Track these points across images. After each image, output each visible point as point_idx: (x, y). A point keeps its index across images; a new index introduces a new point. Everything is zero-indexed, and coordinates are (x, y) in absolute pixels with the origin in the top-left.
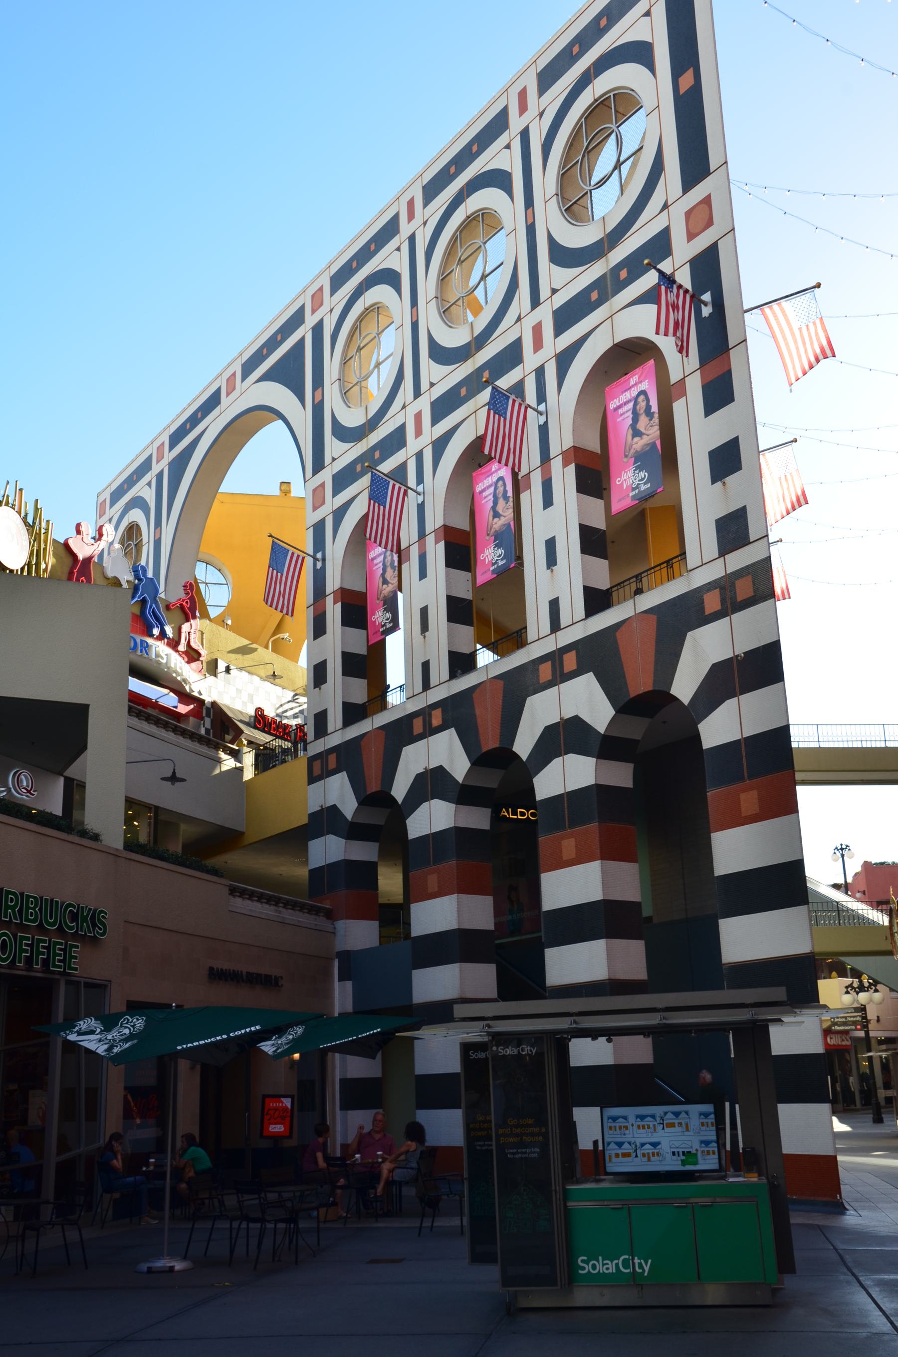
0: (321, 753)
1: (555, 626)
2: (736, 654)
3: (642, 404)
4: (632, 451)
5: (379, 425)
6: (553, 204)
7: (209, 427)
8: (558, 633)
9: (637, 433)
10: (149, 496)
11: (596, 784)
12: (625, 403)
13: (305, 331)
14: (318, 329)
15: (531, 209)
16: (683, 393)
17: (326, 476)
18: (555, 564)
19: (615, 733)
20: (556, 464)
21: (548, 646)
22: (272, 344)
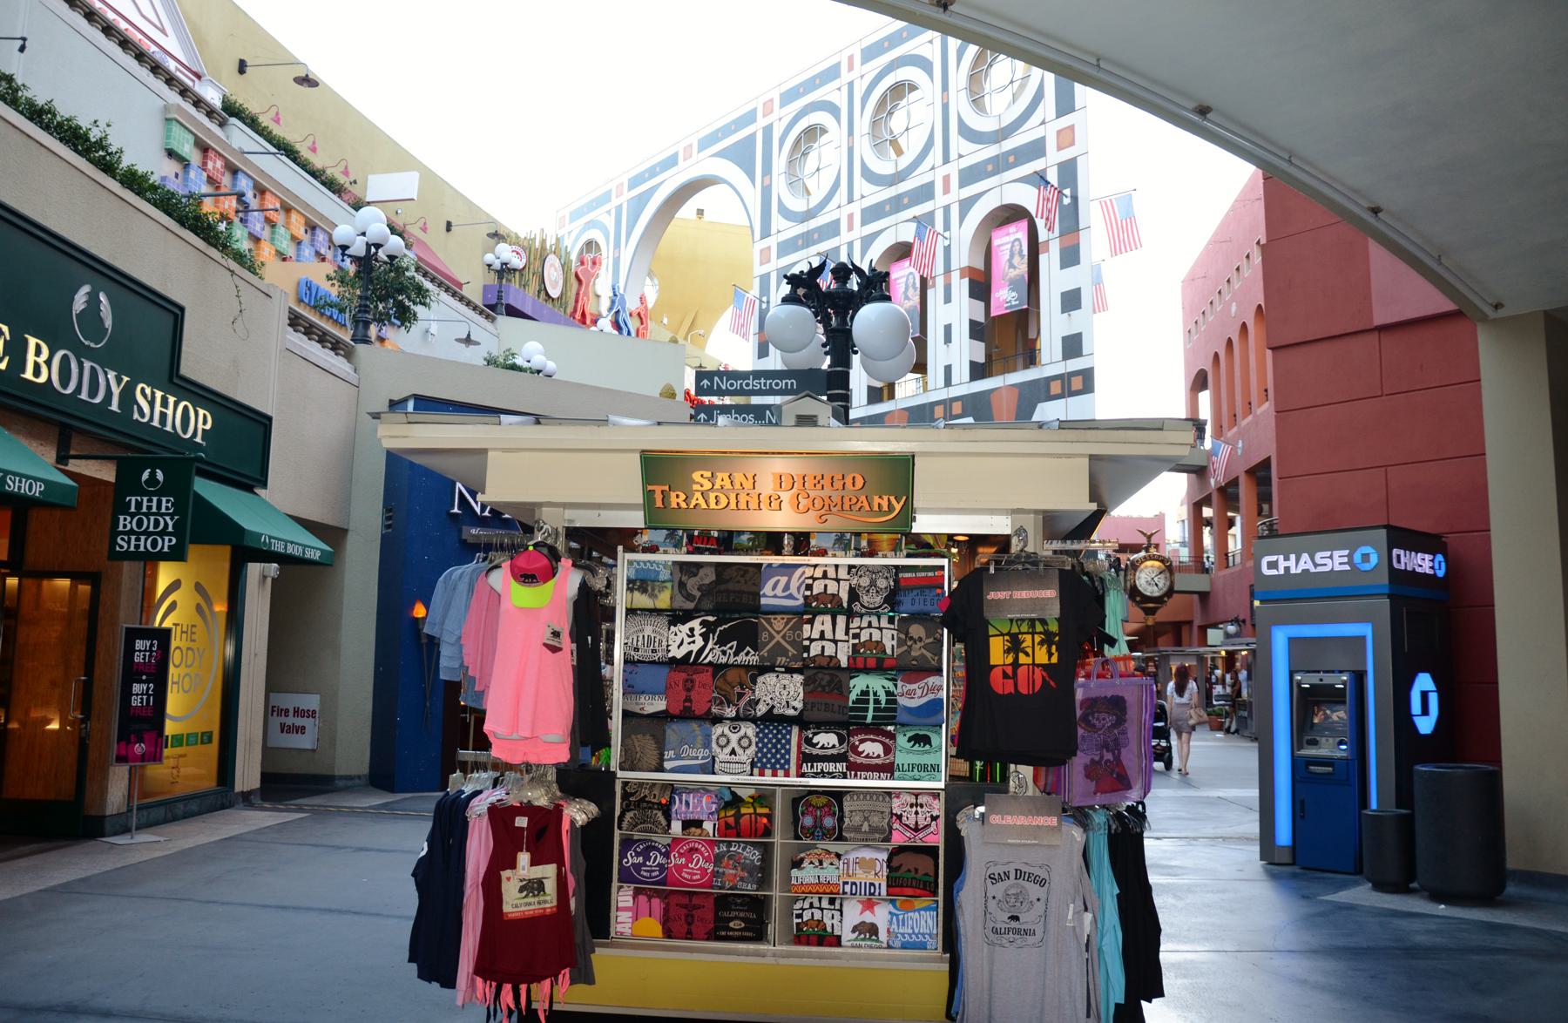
0: (945, 400)
1: (948, 382)
3: (1017, 248)
4: (1008, 277)
6: (964, 95)
9: (1012, 266)
10: (610, 223)
12: (1007, 243)
13: (757, 128)
14: (768, 130)
15: (946, 93)
17: (772, 242)
18: (950, 342)
20: (955, 276)
21: (943, 394)
22: (726, 131)
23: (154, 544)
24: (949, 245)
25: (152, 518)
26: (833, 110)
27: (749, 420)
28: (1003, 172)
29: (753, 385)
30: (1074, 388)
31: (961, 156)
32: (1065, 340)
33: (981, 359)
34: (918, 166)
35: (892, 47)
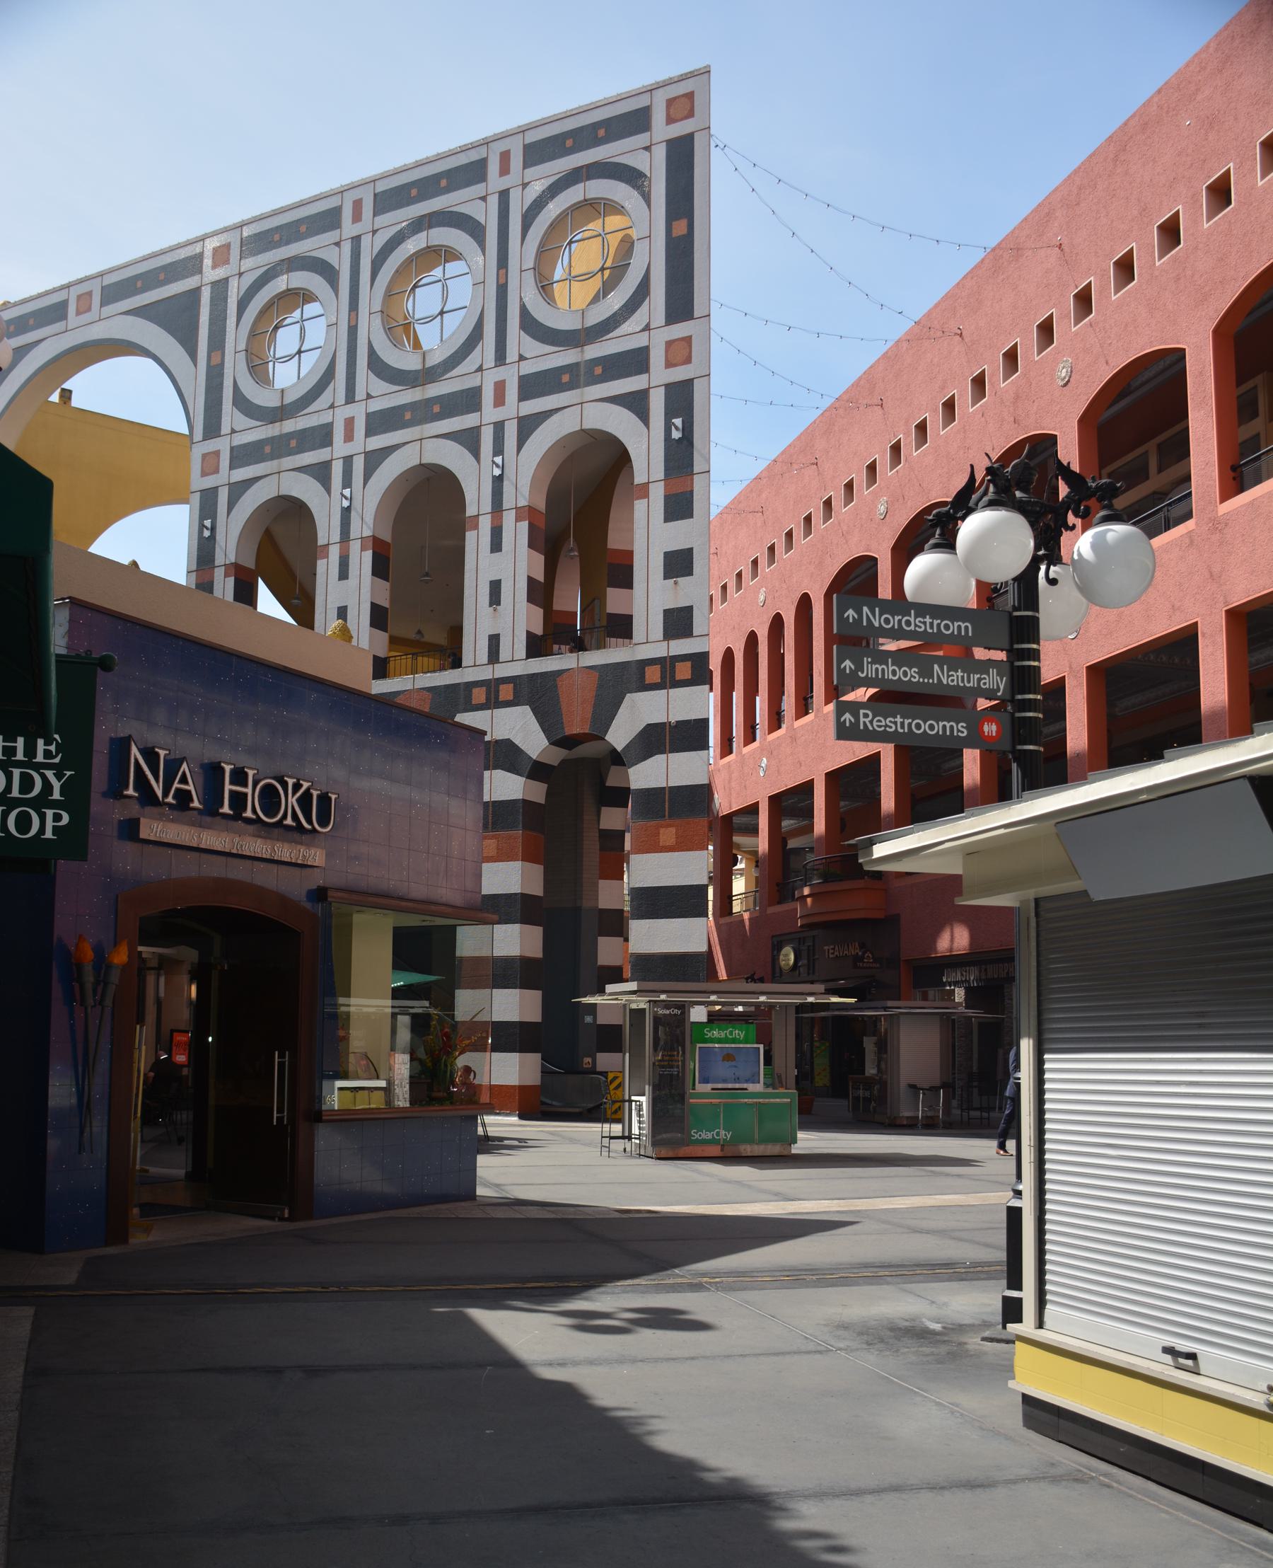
1: (494, 656)
7: (45, 341)
11: (523, 799)
14: (220, 287)
16: (476, 527)
17: (222, 445)
18: (499, 604)
21: (486, 674)
23: (24, 823)
25: (16, 773)
27: (912, 676)
29: (916, 625)
30: (679, 677)
32: (668, 613)
33: (539, 631)
34: (459, 363)
35: (422, 197)
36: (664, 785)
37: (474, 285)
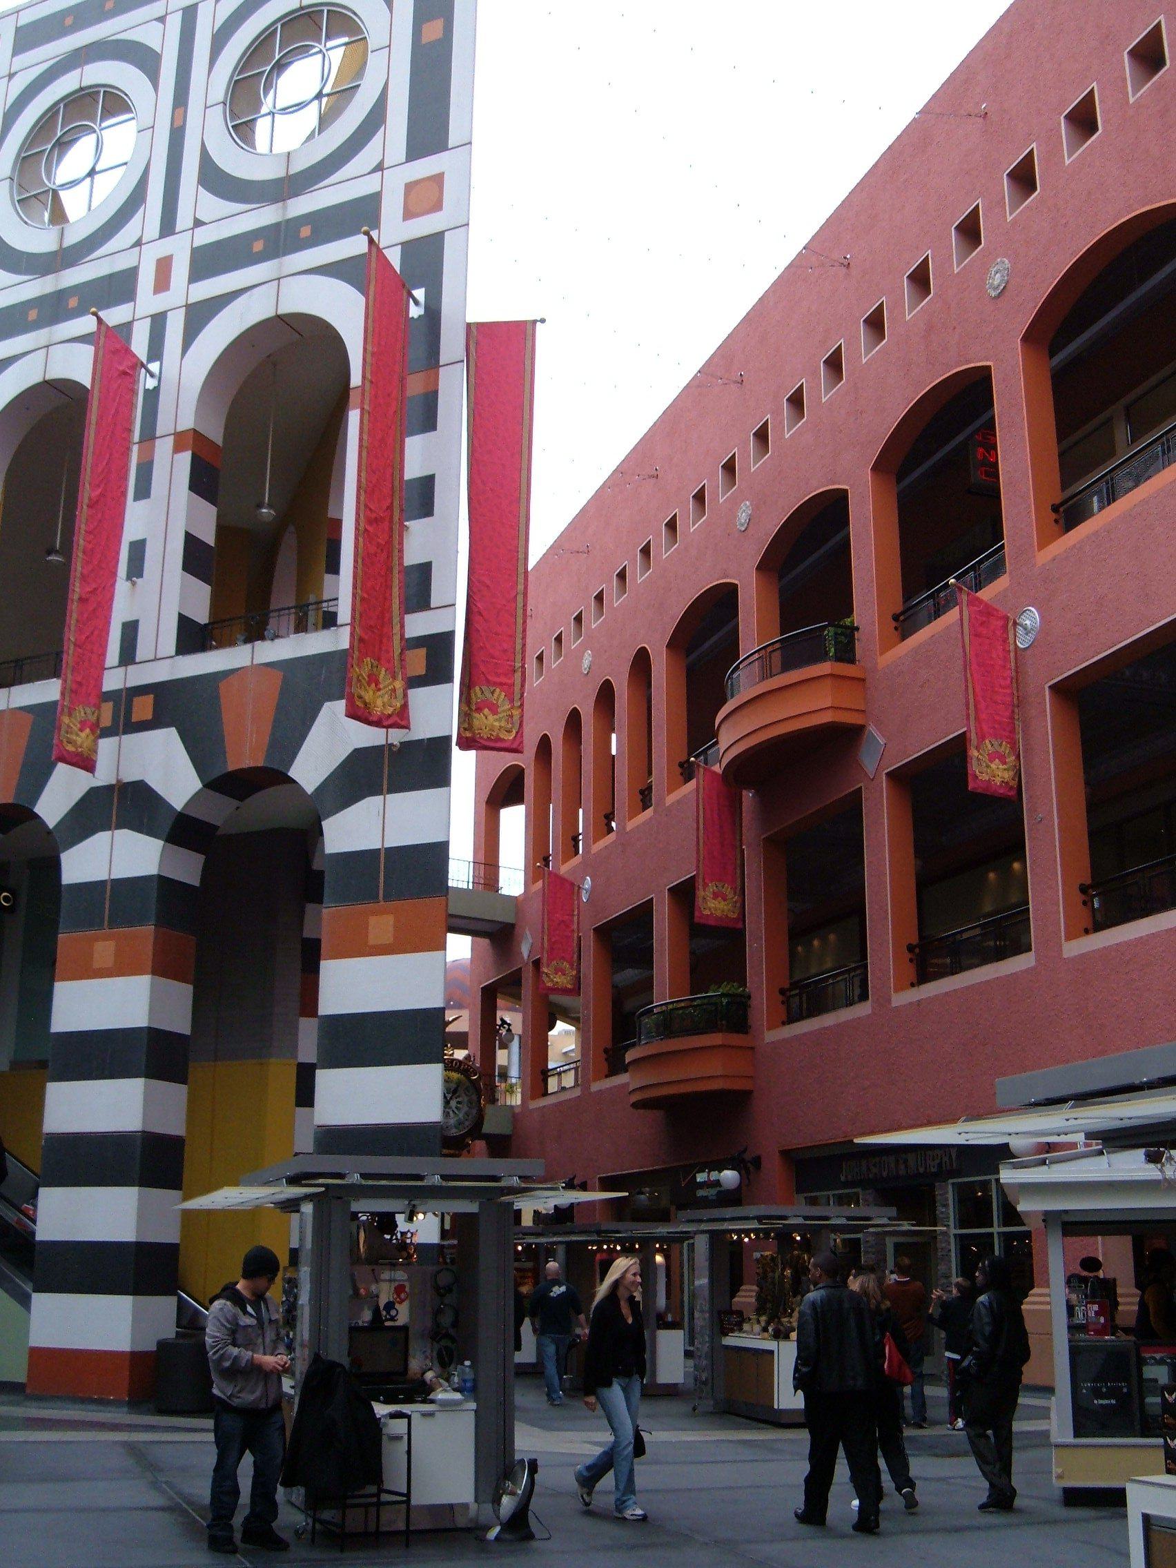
2: (389, 742)
5: (84, 260)
6: (217, 117)
8: (130, 668)
18: (140, 575)
19: (193, 813)
20: (164, 448)
24: (157, 390)
26: (146, 60)
28: (285, 254)
31: (198, 223)
33: (201, 615)
36: (378, 846)
37: (139, 132)
